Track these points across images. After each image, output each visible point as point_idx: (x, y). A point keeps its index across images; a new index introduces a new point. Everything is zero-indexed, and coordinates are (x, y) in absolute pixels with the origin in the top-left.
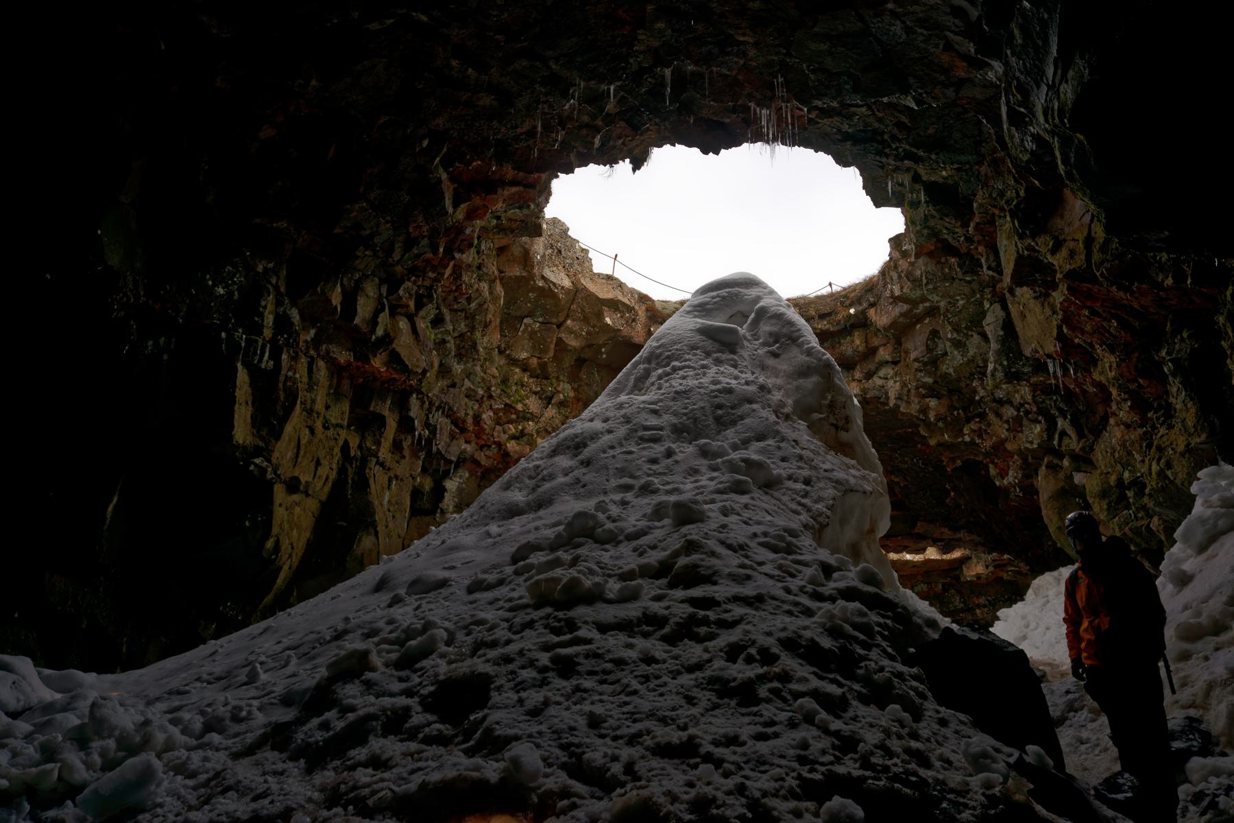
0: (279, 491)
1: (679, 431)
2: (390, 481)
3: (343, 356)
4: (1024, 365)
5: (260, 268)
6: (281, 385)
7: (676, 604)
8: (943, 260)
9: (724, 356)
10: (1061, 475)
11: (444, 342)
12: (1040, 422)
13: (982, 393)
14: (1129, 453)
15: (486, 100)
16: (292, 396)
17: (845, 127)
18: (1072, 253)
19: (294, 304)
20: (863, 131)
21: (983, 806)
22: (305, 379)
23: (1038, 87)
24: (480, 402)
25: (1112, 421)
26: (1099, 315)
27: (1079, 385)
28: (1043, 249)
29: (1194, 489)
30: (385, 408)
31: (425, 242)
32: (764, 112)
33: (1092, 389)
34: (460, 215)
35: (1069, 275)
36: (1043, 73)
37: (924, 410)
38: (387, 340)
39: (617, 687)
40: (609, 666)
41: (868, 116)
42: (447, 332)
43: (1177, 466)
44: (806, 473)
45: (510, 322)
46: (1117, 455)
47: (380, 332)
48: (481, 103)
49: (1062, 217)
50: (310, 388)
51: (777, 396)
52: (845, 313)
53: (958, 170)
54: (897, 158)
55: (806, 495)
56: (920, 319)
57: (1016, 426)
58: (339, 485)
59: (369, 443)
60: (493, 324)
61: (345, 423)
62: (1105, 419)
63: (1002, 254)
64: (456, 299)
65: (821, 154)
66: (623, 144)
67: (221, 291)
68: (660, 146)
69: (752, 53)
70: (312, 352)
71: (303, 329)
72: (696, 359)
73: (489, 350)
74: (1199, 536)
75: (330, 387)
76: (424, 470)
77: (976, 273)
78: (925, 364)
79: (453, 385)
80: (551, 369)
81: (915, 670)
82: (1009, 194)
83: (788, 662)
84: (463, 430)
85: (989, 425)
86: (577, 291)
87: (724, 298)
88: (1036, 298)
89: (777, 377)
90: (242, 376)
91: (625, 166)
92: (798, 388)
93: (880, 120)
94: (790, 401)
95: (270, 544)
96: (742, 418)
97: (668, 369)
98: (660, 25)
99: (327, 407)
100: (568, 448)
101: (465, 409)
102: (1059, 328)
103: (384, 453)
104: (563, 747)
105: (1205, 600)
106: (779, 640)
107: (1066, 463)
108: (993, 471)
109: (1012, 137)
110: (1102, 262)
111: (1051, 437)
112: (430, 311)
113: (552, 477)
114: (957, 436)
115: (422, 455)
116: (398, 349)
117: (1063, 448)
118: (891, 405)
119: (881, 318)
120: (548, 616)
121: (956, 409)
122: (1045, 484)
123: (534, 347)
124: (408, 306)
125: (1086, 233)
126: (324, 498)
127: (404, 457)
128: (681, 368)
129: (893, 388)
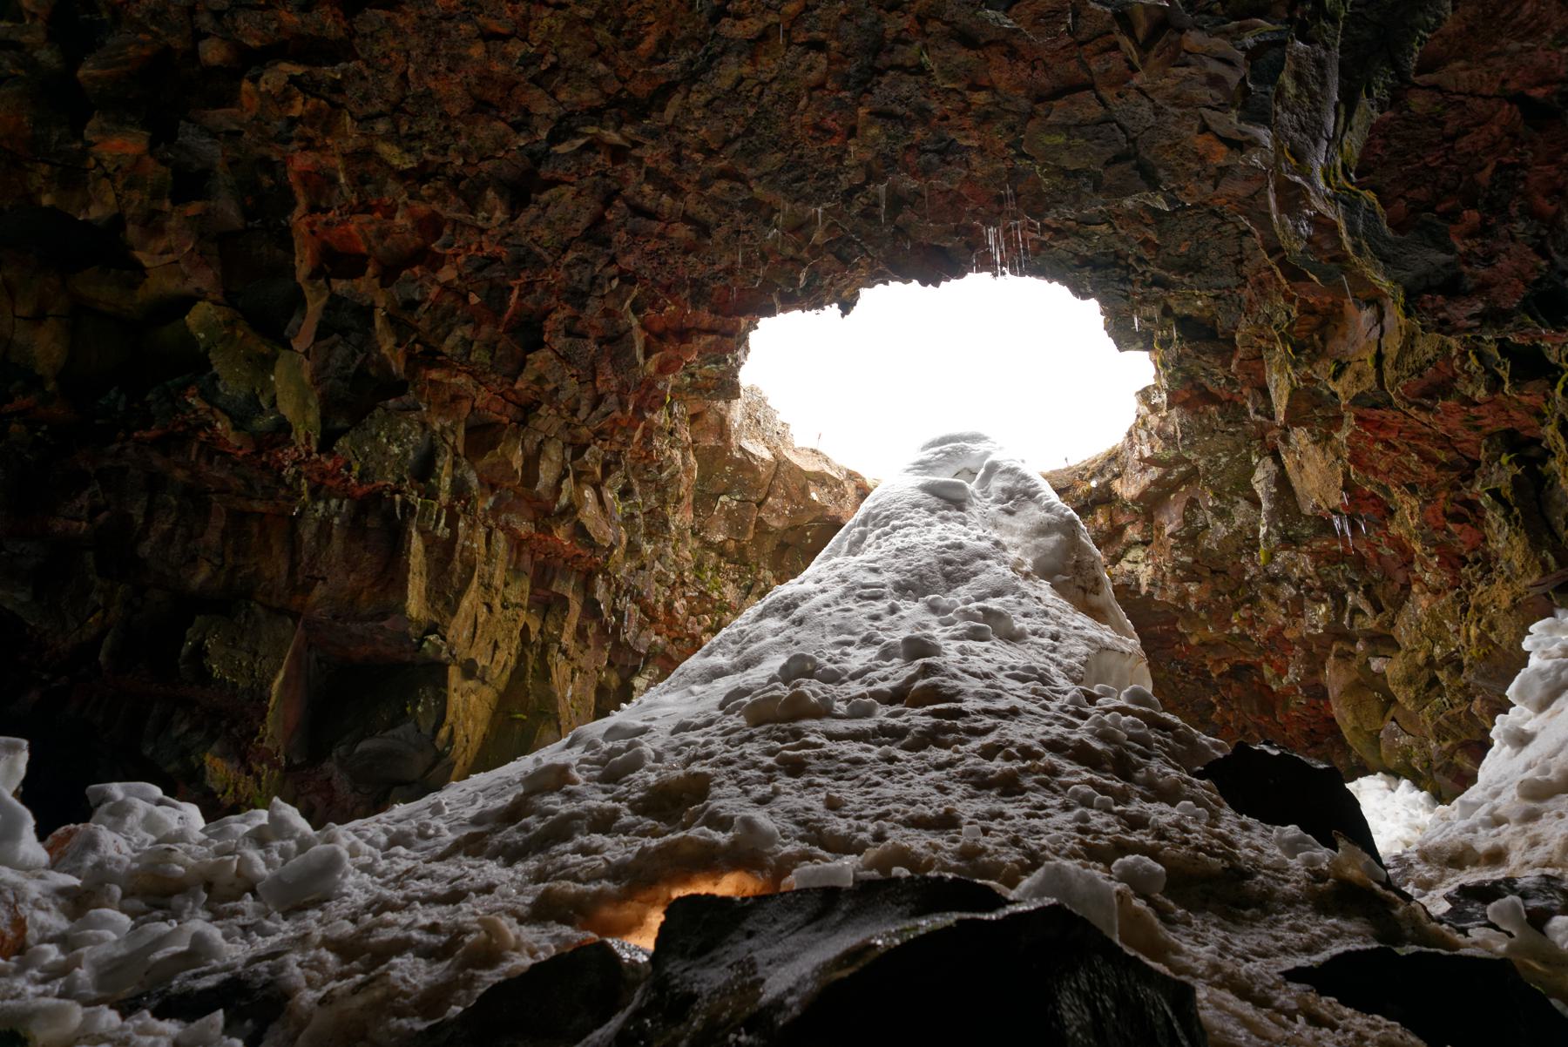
0: (454, 673)
1: (903, 589)
2: (573, 673)
3: (524, 528)
4: (1303, 527)
5: (437, 427)
6: (457, 555)
7: (919, 719)
8: (1201, 409)
9: (950, 514)
10: (1355, 665)
11: (632, 516)
12: (1325, 601)
13: (1252, 571)
14: (1440, 624)
15: (682, 232)
16: (470, 567)
17: (1083, 250)
18: (1359, 376)
19: (472, 466)
20: (1104, 254)
21: (1308, 880)
22: (483, 551)
23: (1316, 143)
24: (672, 588)
25: (1415, 588)
26: (1395, 448)
27: (1373, 547)
28: (1322, 376)
29: (1527, 644)
30: (567, 588)
31: (613, 399)
32: (991, 230)
33: (1387, 551)
34: (651, 368)
35: (1356, 401)
36: (1321, 125)
37: (1184, 597)
38: (571, 510)
39: (856, 782)
40: (844, 765)
41: (1109, 236)
42: (636, 505)
43: (1501, 627)
44: (1053, 628)
45: (704, 501)
46: (1424, 627)
47: (564, 500)
48: (675, 235)
49: (1344, 336)
50: (488, 562)
51: (1013, 555)
52: (1085, 488)
53: (1216, 298)
54: (1143, 284)
55: (1054, 650)
56: (1174, 488)
57: (1296, 609)
58: (518, 674)
59: (551, 628)
60: (686, 501)
61: (525, 603)
62: (1406, 587)
63: (1272, 390)
64: (646, 467)
65: (1056, 284)
66: (831, 284)
67: (396, 450)
68: (871, 286)
69: (976, 161)
70: (490, 522)
71: (482, 495)
72: (921, 517)
73: (681, 533)
74: (1538, 691)
75: (509, 562)
76: (611, 664)
77: (1241, 423)
78: (1182, 540)
79: (643, 567)
80: (751, 553)
81: (1205, 782)
82: (1279, 317)
83: (1050, 758)
84: (654, 620)
85: (1263, 610)
86: (780, 464)
87: (948, 453)
88: (1315, 443)
89: (1012, 535)
90: (416, 543)
91: (833, 310)
92: (1037, 547)
93: (1124, 240)
94: (1029, 561)
95: (443, 733)
96: (975, 574)
97: (887, 529)
98: (874, 131)
99: (506, 585)
100: (777, 610)
101: (657, 595)
102: (1346, 475)
103: (567, 639)
104: (798, 823)
105: (1554, 755)
106: (1042, 742)
107: (1360, 646)
108: (1268, 672)
109: (1283, 226)
110: (1397, 380)
111: (1339, 618)
112: (617, 479)
113: (759, 638)
114: (1223, 628)
115: (609, 645)
116: (584, 520)
117: (1356, 628)
118: (1143, 592)
119: (1128, 489)
120: (770, 730)
121: (1221, 594)
122: (1334, 677)
123: (731, 528)
124: (594, 473)
125: (1375, 349)
126: (501, 687)
127: (588, 647)
128: (900, 527)
129: (1145, 573)
